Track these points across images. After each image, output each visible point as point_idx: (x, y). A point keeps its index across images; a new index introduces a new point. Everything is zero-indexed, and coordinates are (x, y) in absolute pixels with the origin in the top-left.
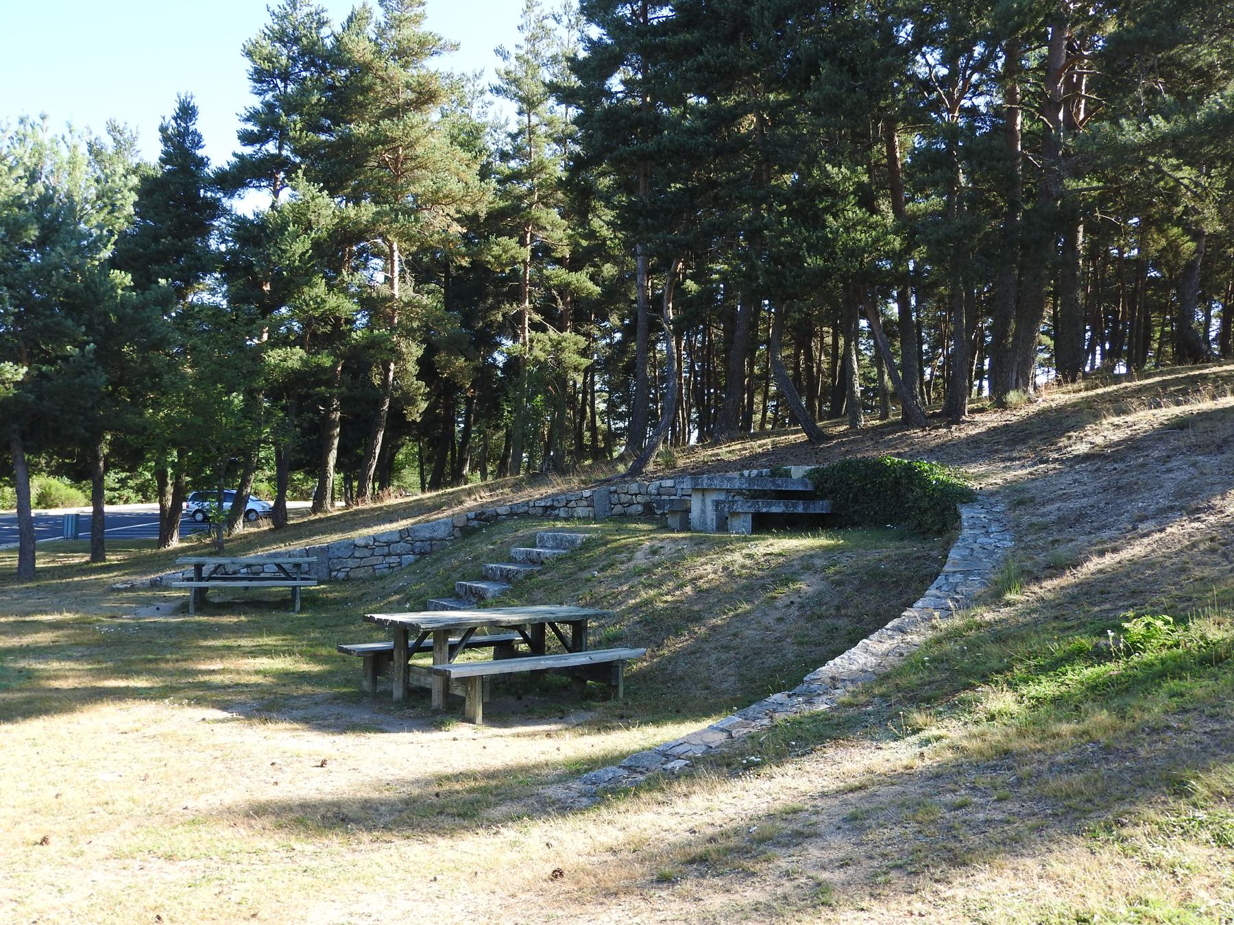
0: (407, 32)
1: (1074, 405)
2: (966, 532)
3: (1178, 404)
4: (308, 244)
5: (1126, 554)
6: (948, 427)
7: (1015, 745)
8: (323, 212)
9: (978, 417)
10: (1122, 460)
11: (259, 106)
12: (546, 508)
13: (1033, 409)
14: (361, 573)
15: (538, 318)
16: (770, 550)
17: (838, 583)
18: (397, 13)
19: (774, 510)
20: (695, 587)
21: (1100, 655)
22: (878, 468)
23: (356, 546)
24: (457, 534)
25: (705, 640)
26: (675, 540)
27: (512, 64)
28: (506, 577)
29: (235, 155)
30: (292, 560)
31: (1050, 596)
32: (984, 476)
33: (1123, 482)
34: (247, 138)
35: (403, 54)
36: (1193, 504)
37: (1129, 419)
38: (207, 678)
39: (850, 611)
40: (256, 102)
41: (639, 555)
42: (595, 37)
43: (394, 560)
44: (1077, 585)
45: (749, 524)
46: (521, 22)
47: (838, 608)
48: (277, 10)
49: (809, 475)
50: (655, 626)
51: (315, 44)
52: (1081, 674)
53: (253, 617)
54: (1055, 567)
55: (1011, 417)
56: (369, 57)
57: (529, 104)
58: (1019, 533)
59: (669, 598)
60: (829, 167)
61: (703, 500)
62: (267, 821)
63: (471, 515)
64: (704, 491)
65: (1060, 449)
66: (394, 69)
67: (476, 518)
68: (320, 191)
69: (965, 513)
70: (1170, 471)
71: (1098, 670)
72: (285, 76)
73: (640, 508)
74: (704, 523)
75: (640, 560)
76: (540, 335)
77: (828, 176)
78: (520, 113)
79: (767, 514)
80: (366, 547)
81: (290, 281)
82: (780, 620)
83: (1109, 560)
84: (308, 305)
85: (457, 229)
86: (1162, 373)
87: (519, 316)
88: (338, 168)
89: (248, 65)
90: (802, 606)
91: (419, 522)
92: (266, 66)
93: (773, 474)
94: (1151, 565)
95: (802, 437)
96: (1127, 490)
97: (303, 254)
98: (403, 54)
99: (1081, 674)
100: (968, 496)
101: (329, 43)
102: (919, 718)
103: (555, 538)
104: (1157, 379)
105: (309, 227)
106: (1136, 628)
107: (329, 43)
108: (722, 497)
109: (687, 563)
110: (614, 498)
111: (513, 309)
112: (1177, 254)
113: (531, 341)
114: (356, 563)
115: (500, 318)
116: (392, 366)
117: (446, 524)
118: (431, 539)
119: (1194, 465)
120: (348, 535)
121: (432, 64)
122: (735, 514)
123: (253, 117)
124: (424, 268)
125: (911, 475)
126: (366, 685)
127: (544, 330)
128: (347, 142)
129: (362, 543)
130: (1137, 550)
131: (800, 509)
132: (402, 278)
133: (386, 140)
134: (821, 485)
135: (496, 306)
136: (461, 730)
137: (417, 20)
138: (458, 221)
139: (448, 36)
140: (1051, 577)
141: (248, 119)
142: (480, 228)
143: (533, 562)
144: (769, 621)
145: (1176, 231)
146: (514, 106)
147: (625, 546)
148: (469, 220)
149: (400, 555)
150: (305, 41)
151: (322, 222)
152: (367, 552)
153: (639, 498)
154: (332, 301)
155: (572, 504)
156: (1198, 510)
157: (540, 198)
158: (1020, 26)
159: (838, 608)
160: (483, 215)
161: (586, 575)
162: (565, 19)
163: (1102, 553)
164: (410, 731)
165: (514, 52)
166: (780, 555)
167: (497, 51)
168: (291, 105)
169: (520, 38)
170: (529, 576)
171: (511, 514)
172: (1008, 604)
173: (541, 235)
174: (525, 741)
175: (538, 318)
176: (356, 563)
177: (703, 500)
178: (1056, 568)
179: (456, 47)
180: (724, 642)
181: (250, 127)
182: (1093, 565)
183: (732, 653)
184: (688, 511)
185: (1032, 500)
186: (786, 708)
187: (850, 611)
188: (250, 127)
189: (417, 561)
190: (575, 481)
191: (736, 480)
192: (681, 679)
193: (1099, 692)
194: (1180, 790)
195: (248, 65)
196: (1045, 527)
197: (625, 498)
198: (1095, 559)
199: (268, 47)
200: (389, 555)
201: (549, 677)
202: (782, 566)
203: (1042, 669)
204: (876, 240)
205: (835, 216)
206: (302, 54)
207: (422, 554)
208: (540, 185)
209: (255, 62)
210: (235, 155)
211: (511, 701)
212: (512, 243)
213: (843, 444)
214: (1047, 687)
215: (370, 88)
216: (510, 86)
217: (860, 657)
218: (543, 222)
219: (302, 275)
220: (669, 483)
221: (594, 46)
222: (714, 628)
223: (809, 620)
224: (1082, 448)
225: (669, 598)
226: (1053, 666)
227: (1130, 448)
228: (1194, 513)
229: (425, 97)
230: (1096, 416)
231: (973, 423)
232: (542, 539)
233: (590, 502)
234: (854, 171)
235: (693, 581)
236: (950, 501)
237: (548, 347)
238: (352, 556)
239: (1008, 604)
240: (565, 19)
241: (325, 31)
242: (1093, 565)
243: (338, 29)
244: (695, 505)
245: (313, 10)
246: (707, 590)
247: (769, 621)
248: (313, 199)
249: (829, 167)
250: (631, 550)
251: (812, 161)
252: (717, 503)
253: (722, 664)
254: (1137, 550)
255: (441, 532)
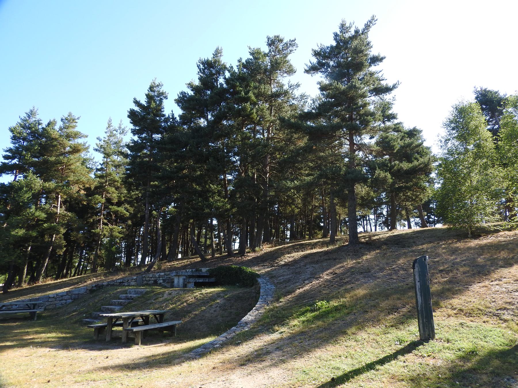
0: (70, 130)
1: (273, 251)
2: (262, 285)
3: (302, 251)
4: (31, 194)
5: (305, 288)
6: (241, 257)
7: (303, 330)
8: (37, 184)
9: (249, 254)
10: (294, 266)
11: (12, 147)
12: (120, 282)
13: (263, 252)
14: (51, 307)
15: (105, 221)
16: (207, 292)
17: (229, 300)
18: (67, 124)
19: (200, 281)
20: (187, 303)
21: (312, 311)
22: (229, 269)
23: (49, 297)
24: (88, 292)
25: (194, 318)
26: (176, 290)
27: (102, 143)
28: (120, 304)
29: (2, 162)
30: (25, 303)
31: (291, 299)
32: (260, 270)
33: (297, 271)
34: (6, 157)
35: (68, 137)
36: (316, 276)
37: (292, 255)
38: (31, 341)
39: (234, 307)
40: (12, 146)
41: (165, 295)
42: (136, 140)
43: (64, 302)
44: (296, 297)
45: (193, 285)
46: (106, 131)
47: (231, 307)
48: (23, 118)
49: (208, 271)
50: (177, 314)
51: (37, 130)
52: (309, 315)
53: (22, 323)
54: (289, 292)
55: (258, 254)
56: (57, 137)
57: (107, 155)
58: (276, 285)
59: (180, 307)
60: (211, 185)
61: (179, 279)
62: (116, 369)
63: (94, 285)
64: (179, 276)
65: (277, 263)
66: (65, 141)
67: (96, 286)
68: (37, 177)
69: (259, 280)
70: (307, 268)
71: (313, 314)
72: (24, 139)
73: (153, 282)
74: (179, 286)
75: (165, 296)
76: (106, 227)
77: (210, 187)
78: (104, 157)
79: (199, 282)
80: (53, 297)
81: (22, 206)
82: (215, 311)
83: (301, 290)
84: (28, 215)
85: (82, 192)
86: (292, 243)
87: (99, 221)
88: (45, 170)
89: (11, 134)
90: (220, 307)
91: (72, 288)
92: (18, 135)
93: (196, 271)
94: (312, 291)
95: (199, 259)
96: (299, 273)
97: (28, 198)
98: (68, 137)
99: (309, 315)
100: (258, 276)
101: (40, 130)
102: (276, 328)
103: (135, 291)
104: (291, 244)
105: (31, 189)
106: (319, 304)
107: (40, 130)
108: (185, 277)
109: (183, 296)
110: (144, 279)
111: (96, 218)
112: (294, 212)
113: (103, 228)
114: (49, 303)
115: (92, 220)
116: (54, 236)
117: (84, 289)
118: (78, 294)
119: (313, 267)
120: (45, 294)
121: (80, 141)
122: (189, 282)
123: (10, 150)
124: (71, 204)
125: (240, 270)
126: (95, 338)
127: (107, 225)
128: (46, 162)
129: (52, 296)
130: (307, 288)
131: (207, 281)
132: (61, 207)
133: (61, 163)
134: (211, 274)
135: (91, 217)
136: (135, 348)
137: (74, 127)
138: (84, 190)
139: (83, 132)
140: (289, 295)
141: (7, 151)
142: (90, 192)
143: (128, 299)
144: (212, 311)
145: (293, 206)
146: (103, 155)
147: (160, 292)
148: (87, 189)
149: (66, 300)
150: (33, 129)
151: (36, 187)
152: (53, 299)
153: (152, 279)
154: (37, 213)
155: (130, 281)
156: (317, 278)
157: (109, 184)
158: (262, 155)
159: (231, 307)
160: (93, 188)
161: (149, 302)
162: (119, 131)
163: (299, 289)
164: (122, 348)
165: (103, 139)
166: (210, 293)
167: (97, 138)
168: (27, 149)
169: (106, 135)
170: (129, 303)
171: (108, 285)
172: (281, 302)
173: (109, 195)
174: (159, 348)
175: (105, 221)
176: (49, 303)
177: (179, 279)
178: (290, 293)
179: (87, 136)
180: (200, 318)
181: (8, 154)
182: (298, 291)
183: (204, 321)
184: (173, 282)
185: (275, 276)
186: (236, 331)
187: (234, 307)
188: (8, 154)
189: (73, 302)
190: (127, 274)
191: (189, 271)
192: (190, 329)
193: (316, 318)
194: (345, 333)
195: (11, 134)
196: (281, 283)
197: (147, 279)
198: (298, 290)
199: (20, 129)
200: (62, 300)
201: (149, 332)
202: (212, 296)
203: (300, 315)
204: (223, 205)
205: (212, 198)
206: (31, 133)
207: (74, 299)
208: (110, 180)
209: (13, 133)
210: (2, 162)
211: (149, 338)
212: (100, 197)
213: (212, 262)
214: (303, 318)
215: (56, 146)
216: (100, 149)
217: (249, 317)
218: (110, 191)
219: (26, 205)
220: (163, 274)
221: (134, 142)
222: (196, 315)
223: (223, 310)
224: (283, 263)
225: (180, 307)
226: (303, 314)
227: (295, 263)
228: (317, 279)
229: (76, 150)
230: (283, 254)
231: (249, 256)
232: (130, 292)
233: (136, 280)
234: (217, 187)
235: (186, 301)
236: (254, 277)
237: (109, 231)
238: (48, 301)
239: (281, 302)
240: (119, 131)
241: (40, 127)
242: (298, 291)
243: (44, 126)
244: (176, 281)
245: (37, 119)
246: (191, 304)
247: (212, 311)
248: (34, 179)
249: (211, 185)
250: (163, 293)
251: (206, 183)
252: (184, 279)
253: (201, 324)
254: (307, 288)
255: (82, 292)
